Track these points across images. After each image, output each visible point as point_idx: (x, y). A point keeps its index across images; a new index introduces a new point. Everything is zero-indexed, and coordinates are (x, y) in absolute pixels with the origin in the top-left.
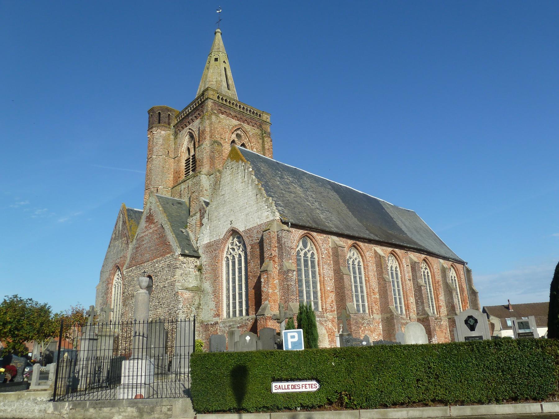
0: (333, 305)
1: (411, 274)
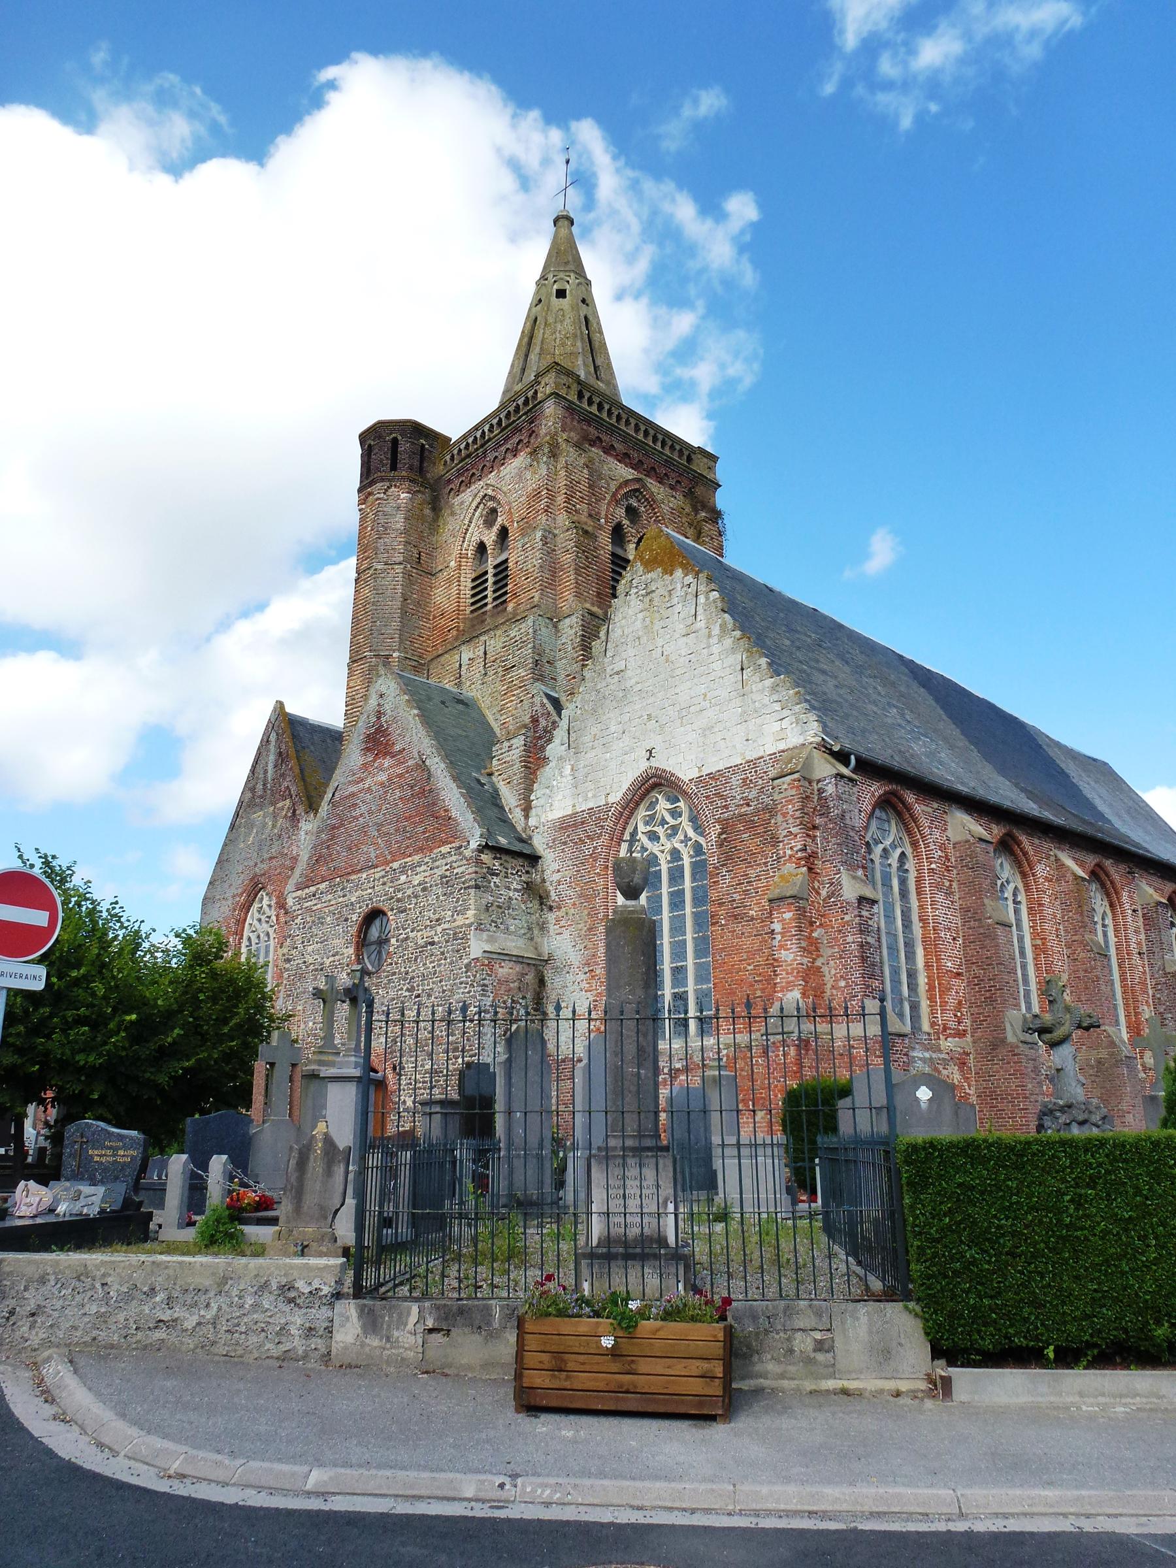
0: (962, 1015)
1: (1143, 937)
